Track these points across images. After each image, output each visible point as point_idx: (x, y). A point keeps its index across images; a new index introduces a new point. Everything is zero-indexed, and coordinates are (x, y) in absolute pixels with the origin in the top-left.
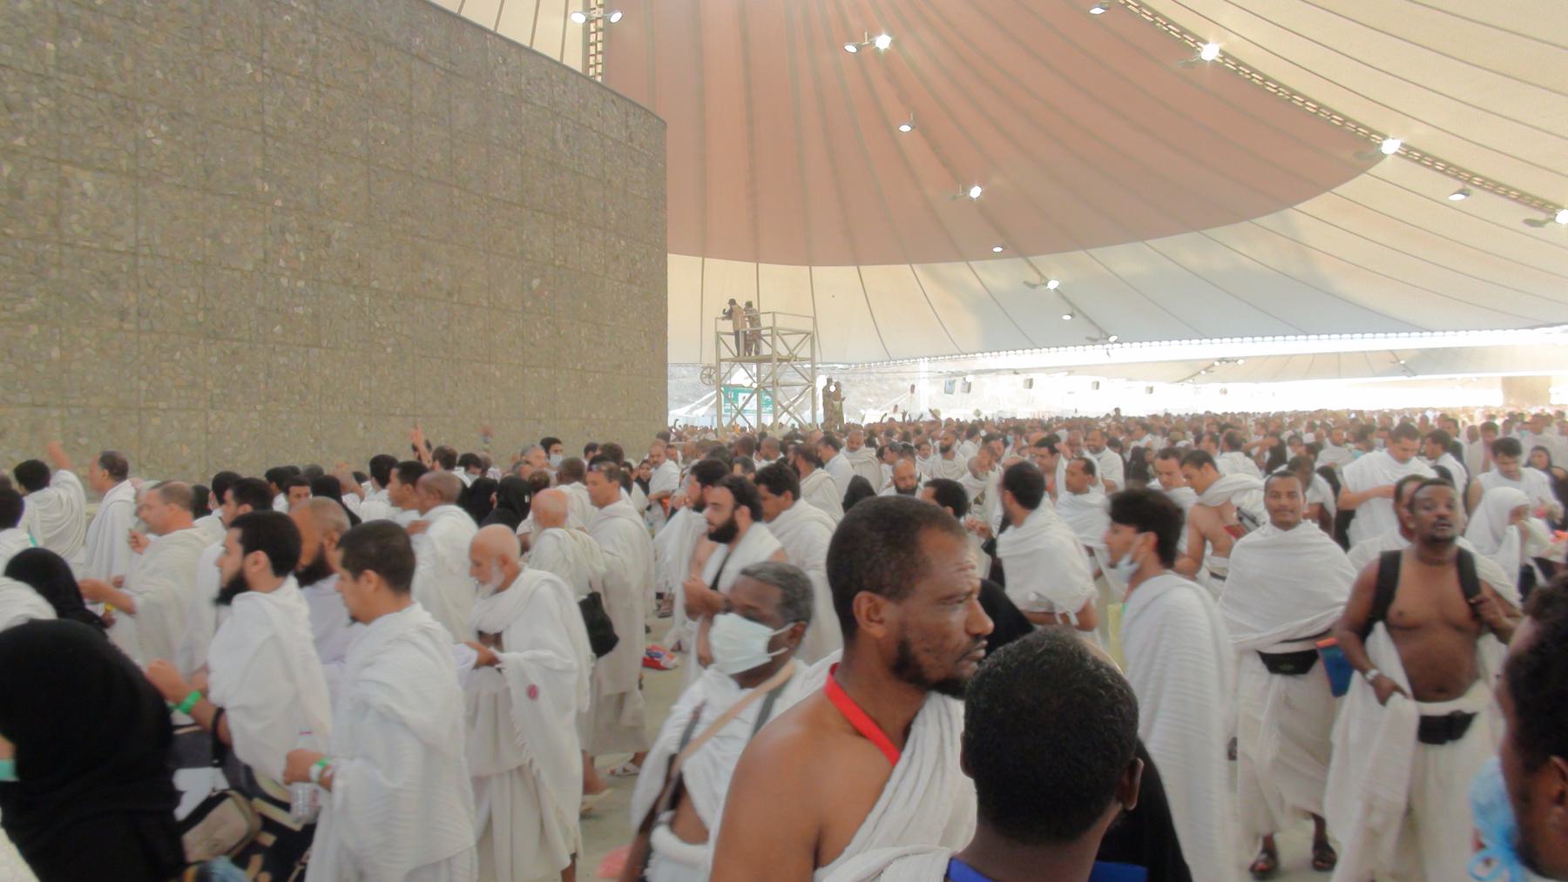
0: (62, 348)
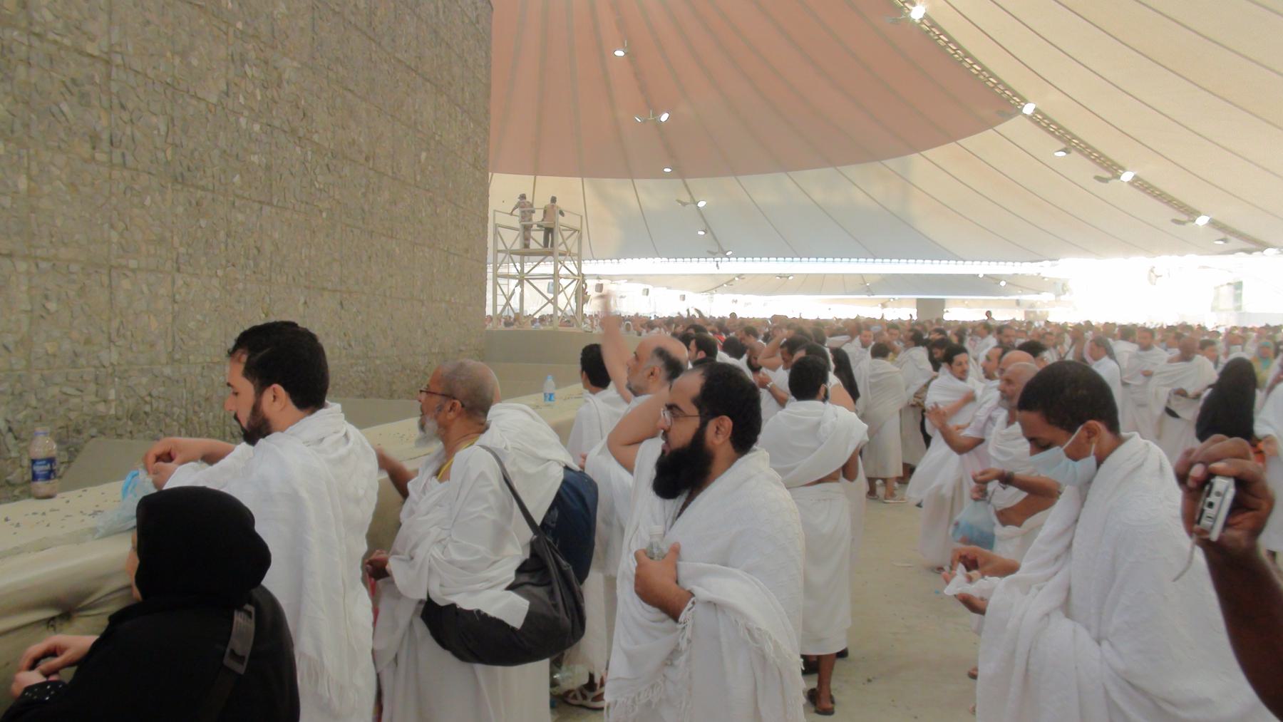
0: (30, 178)
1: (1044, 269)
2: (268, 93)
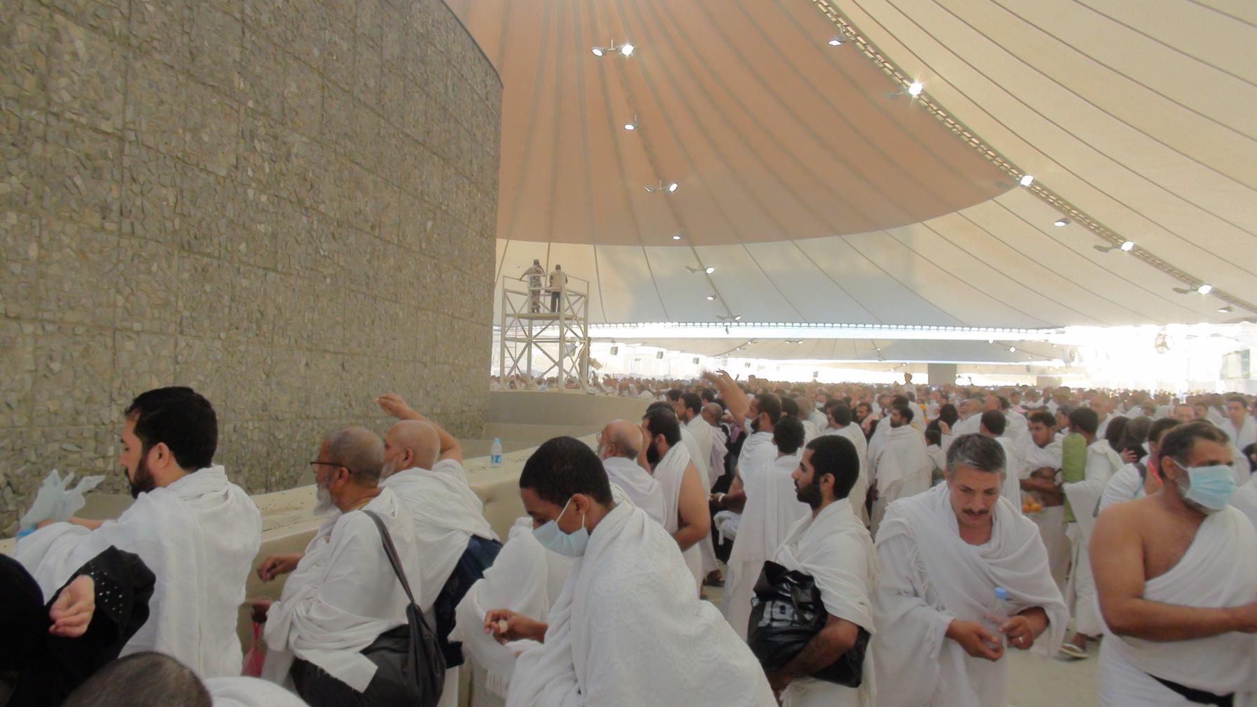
0: (41, 246)
1: (1052, 337)
2: (277, 166)
